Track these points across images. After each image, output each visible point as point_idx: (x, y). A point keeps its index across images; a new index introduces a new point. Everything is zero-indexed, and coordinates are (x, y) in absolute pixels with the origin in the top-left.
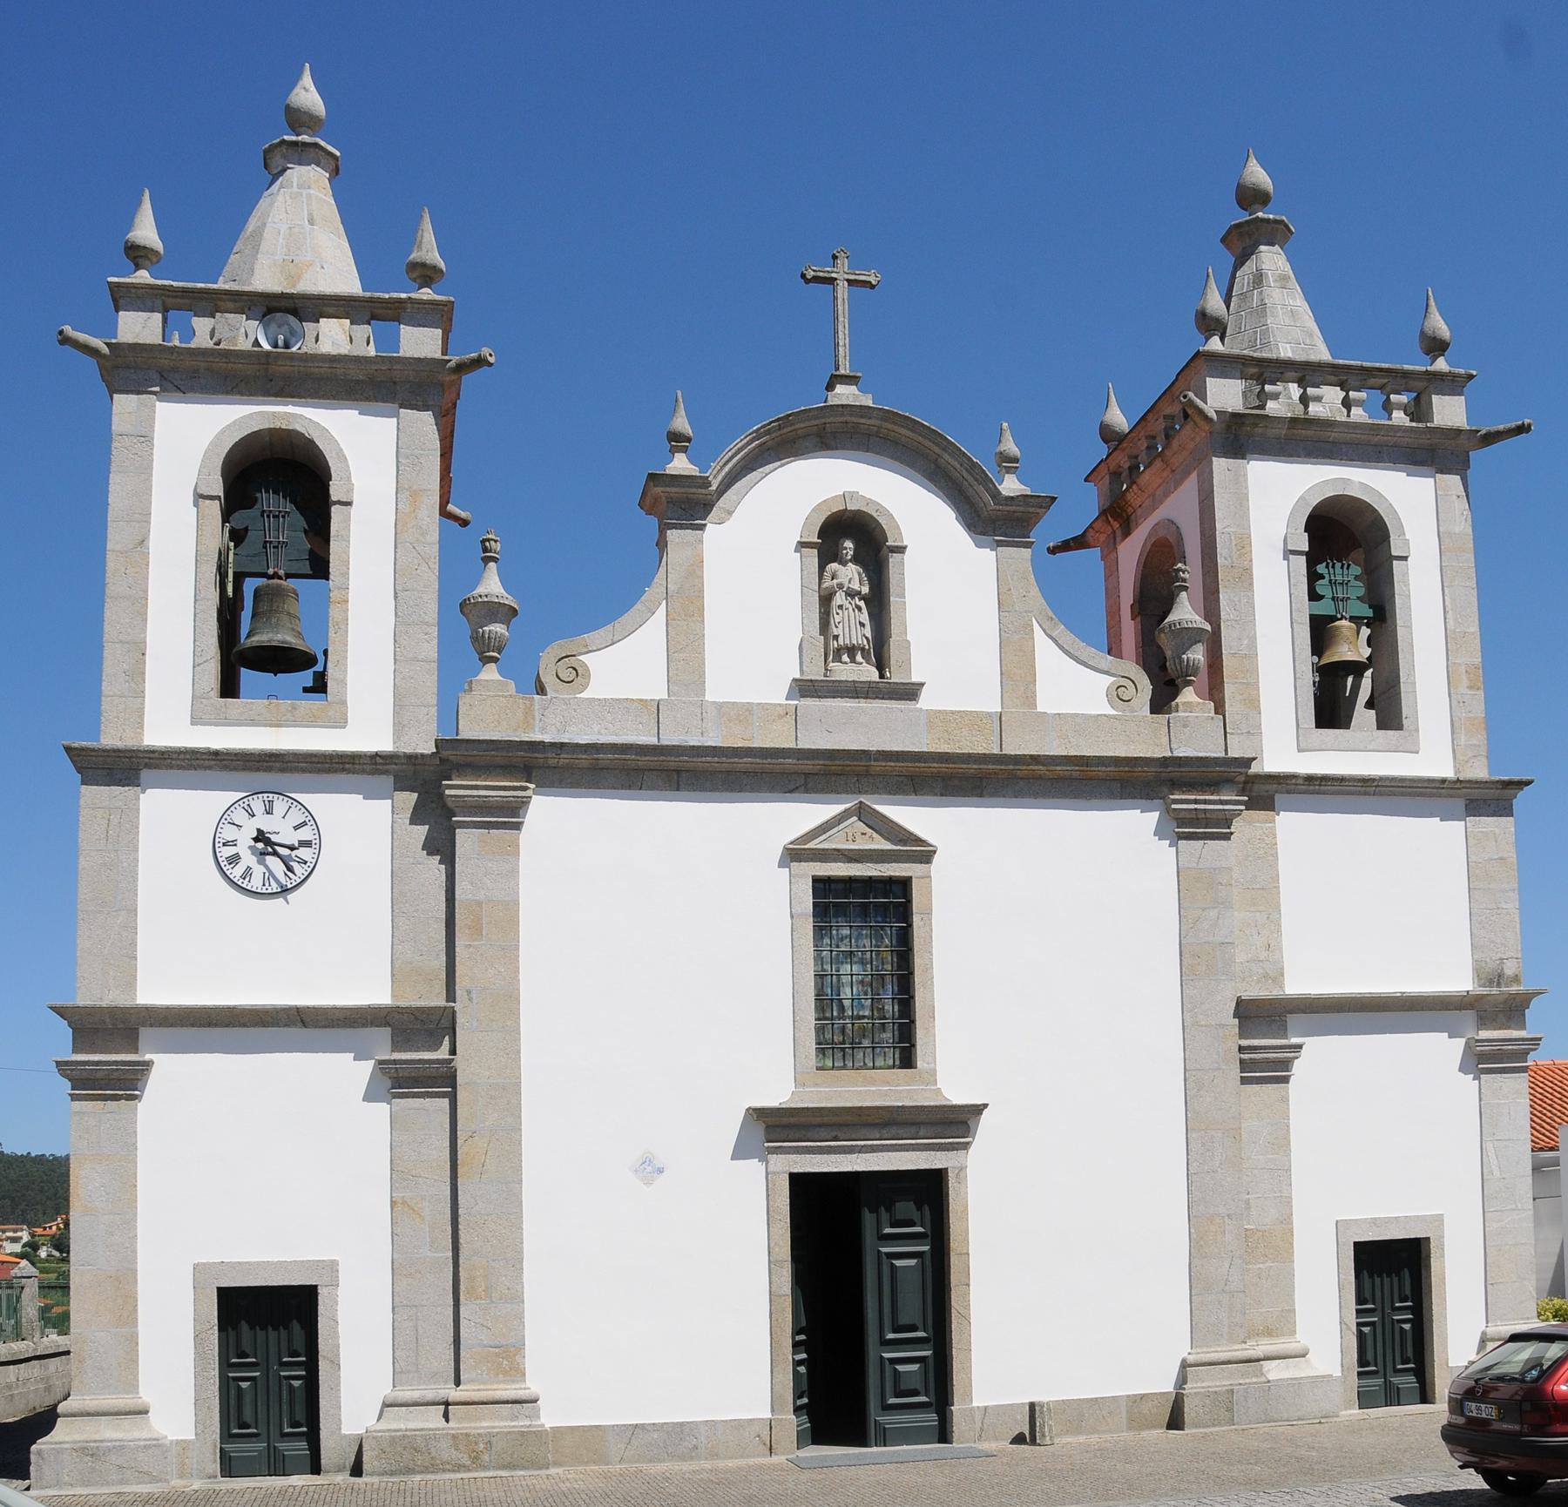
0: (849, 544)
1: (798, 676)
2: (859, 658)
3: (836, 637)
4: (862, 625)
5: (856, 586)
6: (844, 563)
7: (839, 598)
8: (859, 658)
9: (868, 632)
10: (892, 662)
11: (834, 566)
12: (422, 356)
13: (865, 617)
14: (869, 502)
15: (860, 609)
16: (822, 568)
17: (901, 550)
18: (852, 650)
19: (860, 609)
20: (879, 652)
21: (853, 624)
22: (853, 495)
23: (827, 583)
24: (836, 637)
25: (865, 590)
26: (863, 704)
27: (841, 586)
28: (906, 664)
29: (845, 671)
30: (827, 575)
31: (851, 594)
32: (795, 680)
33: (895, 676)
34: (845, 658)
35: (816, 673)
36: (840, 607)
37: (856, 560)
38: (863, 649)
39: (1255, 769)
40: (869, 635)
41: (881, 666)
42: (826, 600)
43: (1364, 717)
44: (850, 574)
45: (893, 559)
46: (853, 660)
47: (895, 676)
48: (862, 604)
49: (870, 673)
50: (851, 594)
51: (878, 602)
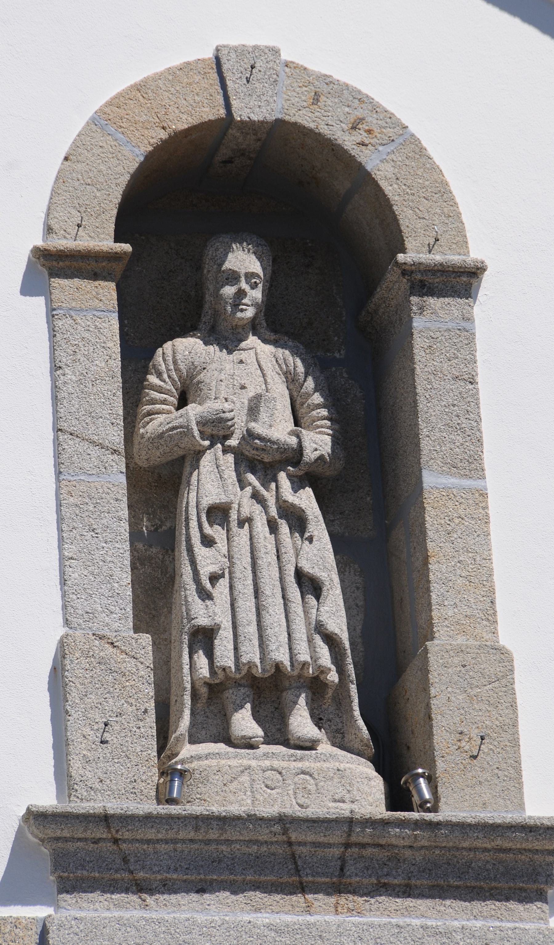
0: (243, 260)
1: (47, 799)
2: (301, 722)
3: (204, 638)
4: (310, 585)
5: (278, 427)
6: (227, 338)
7: (213, 480)
8: (301, 722)
9: (334, 612)
10: (442, 738)
11: (187, 349)
12: (52, 762)
13: (319, 554)
14: (322, 89)
15: (298, 521)
16: (137, 356)
17: (461, 281)
18: (269, 691)
19: (298, 521)
20: (383, 689)
21: (268, 582)
22: (259, 61)
23: (162, 419)
24: (204, 638)
25: (318, 443)
26: (324, 914)
27: (216, 430)
28: (499, 743)
29: (245, 779)
30: (160, 383)
31: (259, 461)
32: (36, 818)
33: (460, 799)
34: (244, 722)
35: (123, 786)
36: (219, 513)
37: (275, 323)
38: (316, 686)
39: (330, 453)
40: (337, 622)
41: (396, 753)
42: (157, 486)
43: (473, 331)
44: (253, 382)
45: (430, 320)
46: (277, 732)
47: (460, 799)
48: (306, 500)
49: (350, 786)
50: (259, 461)
51: (372, 488)
